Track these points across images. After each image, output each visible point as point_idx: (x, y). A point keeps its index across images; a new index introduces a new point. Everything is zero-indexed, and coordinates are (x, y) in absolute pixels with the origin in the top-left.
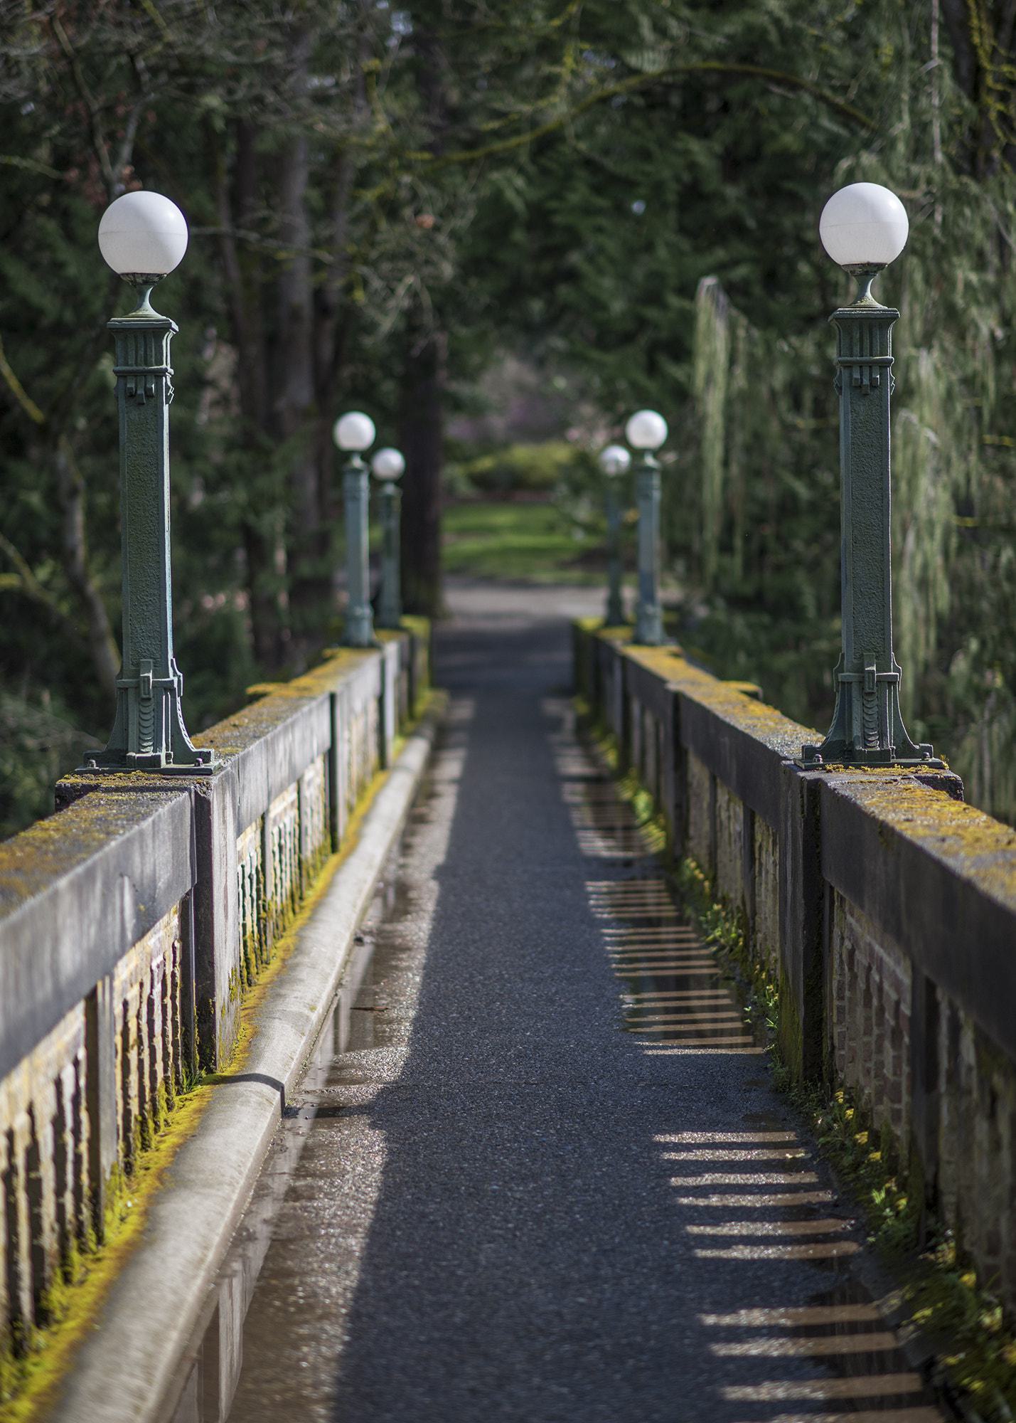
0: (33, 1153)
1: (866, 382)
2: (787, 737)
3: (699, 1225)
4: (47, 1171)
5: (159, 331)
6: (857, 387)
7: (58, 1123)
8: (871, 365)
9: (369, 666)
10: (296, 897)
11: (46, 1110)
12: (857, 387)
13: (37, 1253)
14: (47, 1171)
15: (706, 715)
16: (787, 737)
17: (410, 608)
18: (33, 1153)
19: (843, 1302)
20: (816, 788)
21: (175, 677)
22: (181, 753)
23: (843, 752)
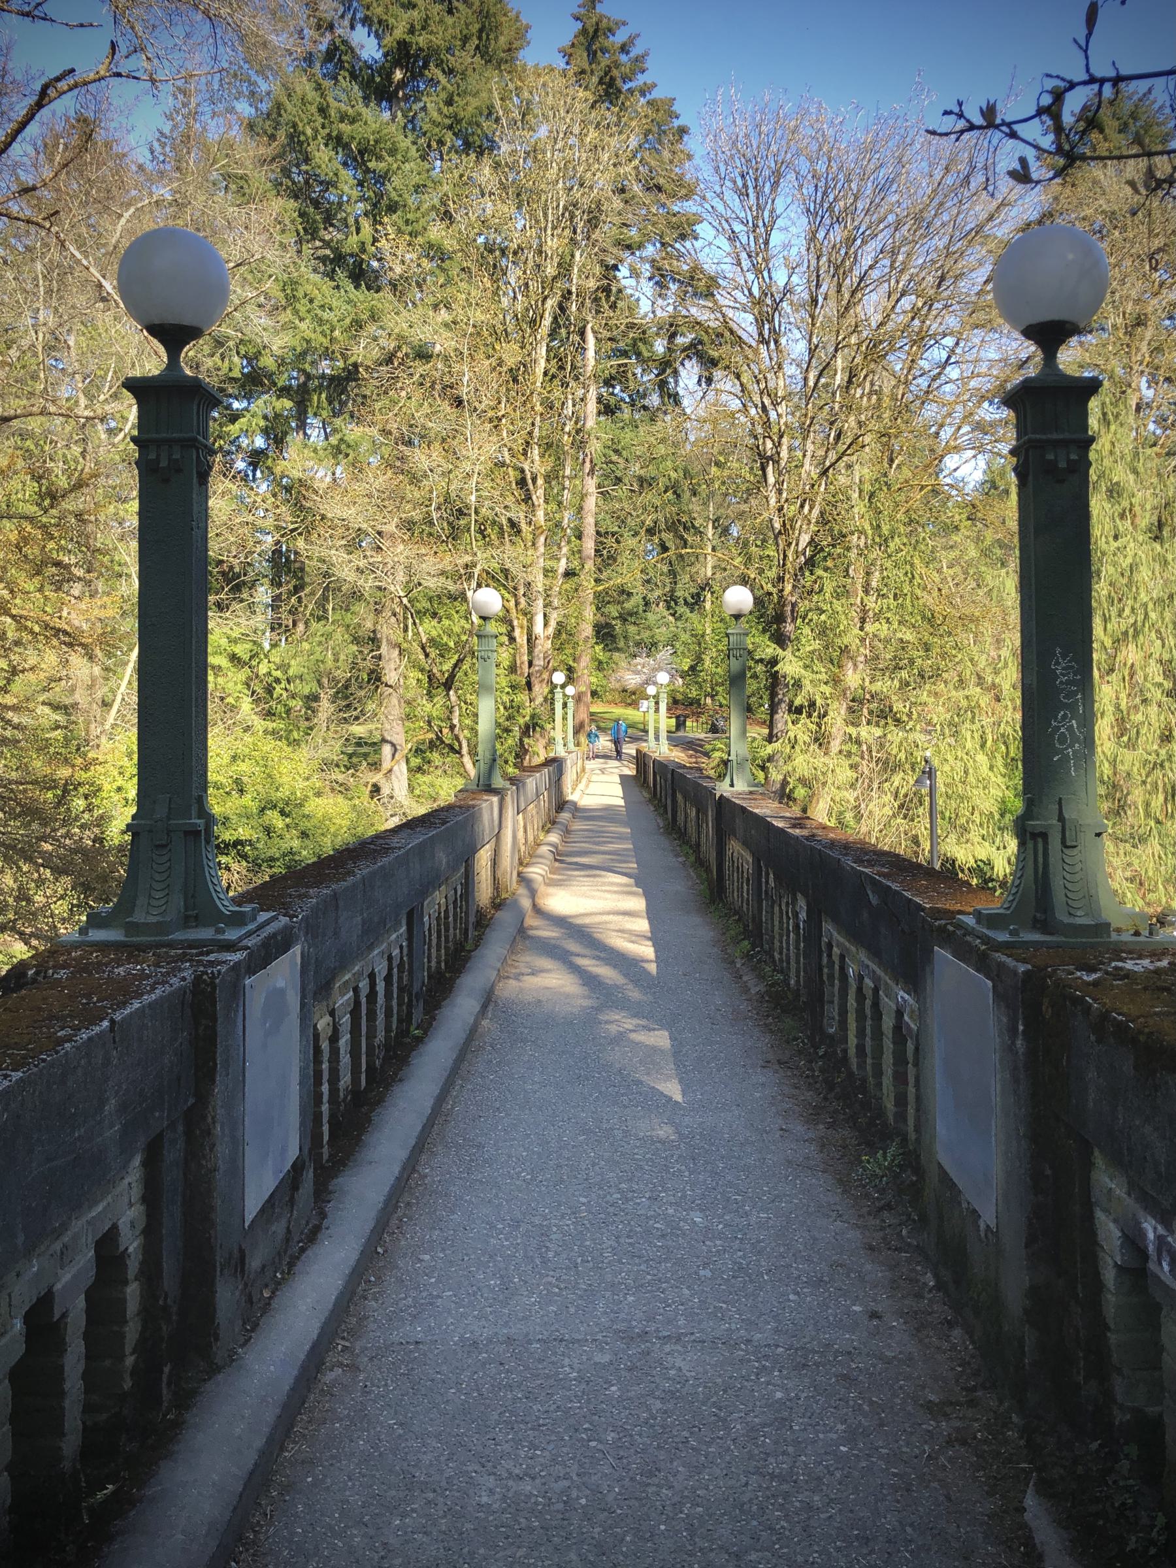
0: (446, 911)
1: (164, 463)
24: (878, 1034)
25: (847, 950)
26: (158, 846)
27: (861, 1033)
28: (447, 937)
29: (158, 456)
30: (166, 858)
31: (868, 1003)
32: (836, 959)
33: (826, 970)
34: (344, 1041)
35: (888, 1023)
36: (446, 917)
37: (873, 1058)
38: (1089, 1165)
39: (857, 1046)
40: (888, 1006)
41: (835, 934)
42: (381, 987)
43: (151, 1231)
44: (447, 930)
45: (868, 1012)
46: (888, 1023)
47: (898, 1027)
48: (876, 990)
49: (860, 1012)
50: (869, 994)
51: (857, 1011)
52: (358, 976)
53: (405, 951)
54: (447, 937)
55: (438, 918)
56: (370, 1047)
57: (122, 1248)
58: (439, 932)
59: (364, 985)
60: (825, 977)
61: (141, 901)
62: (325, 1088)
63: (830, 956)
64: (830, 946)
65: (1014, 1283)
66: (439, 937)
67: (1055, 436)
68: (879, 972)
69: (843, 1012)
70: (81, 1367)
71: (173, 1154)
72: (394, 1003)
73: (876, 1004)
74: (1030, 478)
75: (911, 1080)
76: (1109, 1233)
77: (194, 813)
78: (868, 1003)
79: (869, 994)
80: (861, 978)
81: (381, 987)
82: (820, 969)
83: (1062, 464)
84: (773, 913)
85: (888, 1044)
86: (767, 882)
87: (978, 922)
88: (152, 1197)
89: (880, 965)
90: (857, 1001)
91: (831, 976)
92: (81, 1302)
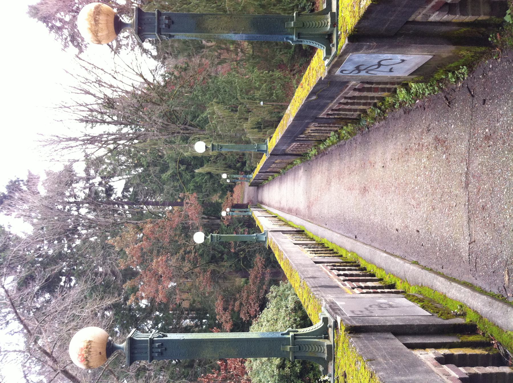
0: (313, 251)
1: (159, 350)
2: (265, 158)
3: (477, 355)
4: (315, 249)
5: (212, 236)
6: (221, 148)
7: (309, 248)
8: (152, 348)
9: (254, 212)
10: (283, 221)
11: (308, 249)
12: (221, 148)
13: (325, 251)
14: (315, 249)
15: (262, 169)
16: (265, 158)
17: (247, 208)
18: (313, 251)
19: (285, 108)
20: (271, 154)
21: (255, 234)
22: (265, 234)
23: (266, 151)
24: (360, 98)
25: (330, 108)
26: (300, 349)
27: (359, 104)
28: (321, 251)
29: (156, 352)
30: (304, 346)
31: (349, 101)
32: (332, 113)
33: (336, 116)
34: (362, 284)
35: (357, 94)
36: (314, 251)
37: (368, 100)
38: (414, 22)
39: (363, 105)
40: (351, 93)
41: (324, 113)
42: (342, 272)
43: (437, 346)
44: (319, 251)
45: (352, 101)
46: (357, 94)
47: (359, 90)
48: (346, 98)
49: (352, 104)
50: (346, 101)
51: (351, 105)
52: (340, 280)
53: (329, 264)
54: (321, 251)
55: (316, 254)
56: (363, 276)
57: (442, 356)
58: (320, 253)
59: (342, 278)
60: (338, 117)
61: (319, 355)
62: (379, 290)
63: (331, 115)
64: (328, 115)
65: (446, 51)
66: (321, 253)
67: (156, 24)
68: (339, 97)
69: (350, 110)
70: (482, 368)
71: (411, 340)
72: (346, 268)
73: (350, 98)
74: (171, 34)
75: (377, 86)
76: (434, 17)
77: (287, 336)
78: (349, 101)
79: (346, 101)
80: (340, 103)
81: (342, 272)
82: (335, 118)
83: (167, 21)
84: (314, 136)
85: (365, 94)
86: (303, 138)
87: (328, 58)
88: (423, 346)
89: (337, 96)
90: (348, 105)
91: (338, 115)
92: (461, 369)
